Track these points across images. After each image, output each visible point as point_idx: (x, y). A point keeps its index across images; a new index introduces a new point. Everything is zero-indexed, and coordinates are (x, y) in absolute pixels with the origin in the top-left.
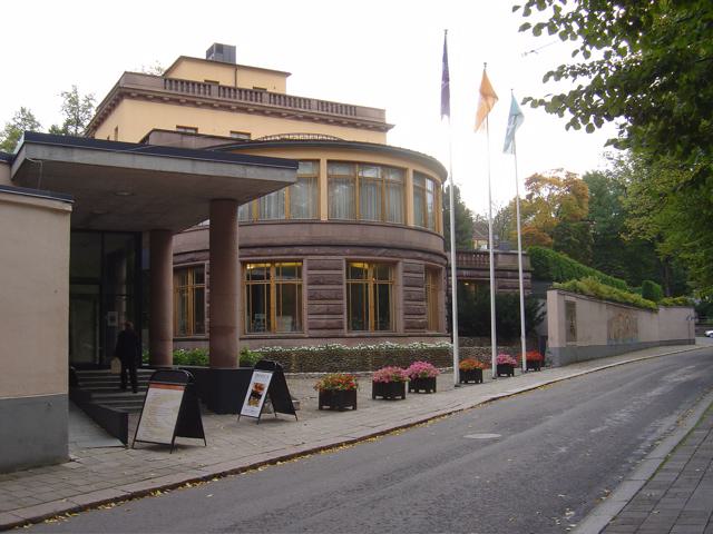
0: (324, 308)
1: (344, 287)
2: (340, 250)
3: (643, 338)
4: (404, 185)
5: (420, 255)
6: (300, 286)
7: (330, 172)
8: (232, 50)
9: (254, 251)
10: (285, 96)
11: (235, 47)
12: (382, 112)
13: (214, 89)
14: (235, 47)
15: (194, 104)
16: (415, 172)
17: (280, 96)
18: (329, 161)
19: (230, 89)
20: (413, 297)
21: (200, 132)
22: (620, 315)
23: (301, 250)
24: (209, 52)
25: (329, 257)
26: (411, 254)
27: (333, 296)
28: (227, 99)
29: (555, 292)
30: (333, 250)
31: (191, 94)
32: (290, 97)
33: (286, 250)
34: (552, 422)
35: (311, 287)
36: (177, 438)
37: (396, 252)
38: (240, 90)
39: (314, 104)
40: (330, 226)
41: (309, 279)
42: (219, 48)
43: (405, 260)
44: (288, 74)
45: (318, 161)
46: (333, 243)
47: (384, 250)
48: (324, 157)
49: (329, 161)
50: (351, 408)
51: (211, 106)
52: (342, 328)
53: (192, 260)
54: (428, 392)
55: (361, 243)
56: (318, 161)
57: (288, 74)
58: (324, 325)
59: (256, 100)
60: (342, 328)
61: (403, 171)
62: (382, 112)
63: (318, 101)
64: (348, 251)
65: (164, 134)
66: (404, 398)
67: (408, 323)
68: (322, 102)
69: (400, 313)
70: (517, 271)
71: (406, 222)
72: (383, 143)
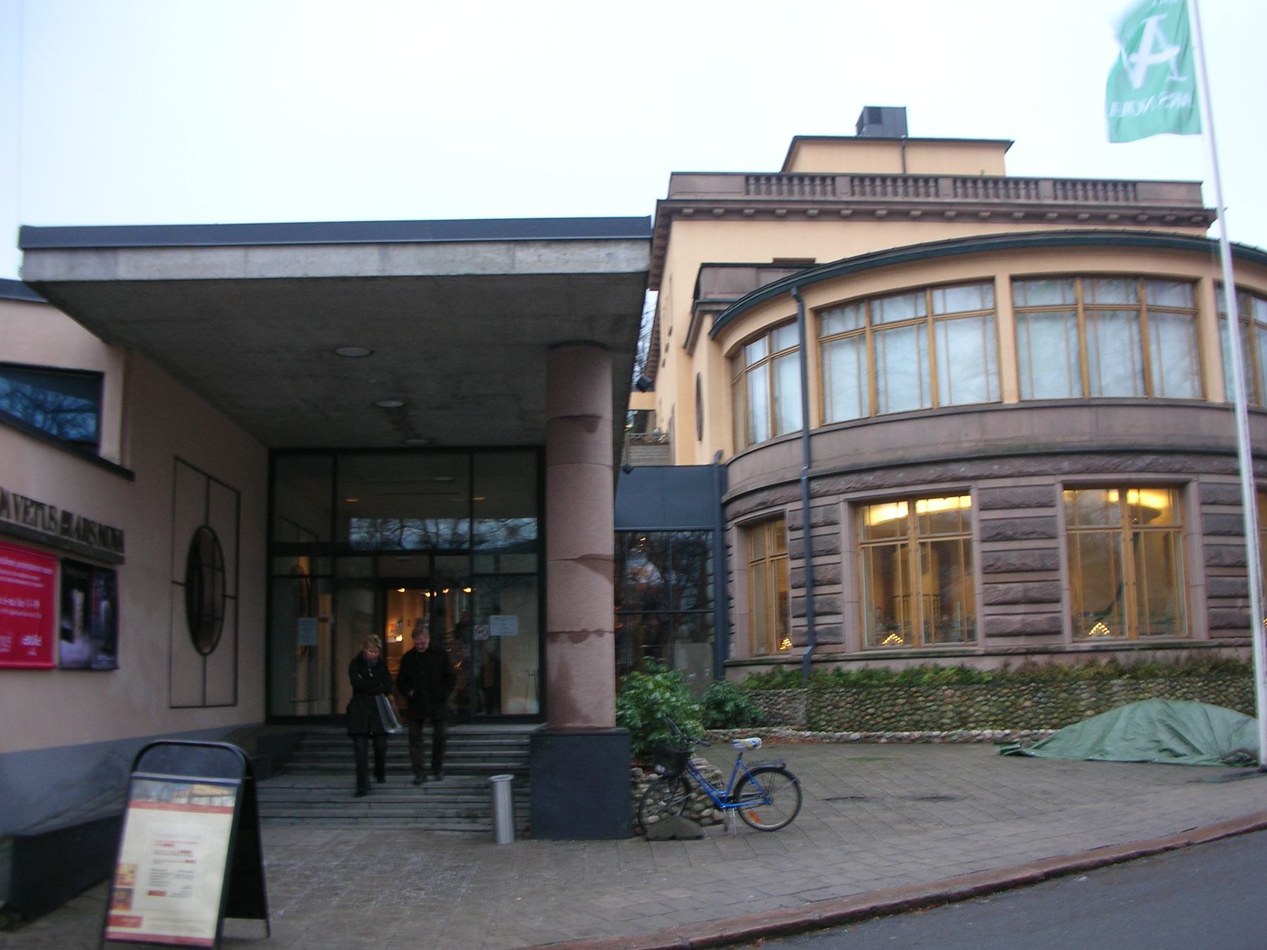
0: (1017, 590)
1: (1061, 543)
2: (1048, 465)
6: (968, 544)
7: (1020, 303)
9: (869, 478)
10: (1006, 181)
11: (903, 111)
14: (903, 111)
17: (996, 181)
18: (1014, 279)
19: (894, 179)
20: (1228, 561)
23: (962, 469)
24: (860, 125)
25: (1023, 481)
27: (1037, 565)
28: (869, 198)
30: (1033, 465)
31: (796, 197)
32: (1017, 181)
33: (932, 472)
34: (554, 945)
35: (989, 546)
36: (227, 921)
37: (1178, 462)
38: (916, 179)
39: (1046, 189)
40: (1023, 416)
41: (983, 530)
42: (873, 115)
43: (1205, 478)
45: (991, 280)
46: (1031, 450)
48: (1002, 271)
49: (1014, 279)
52: (1058, 632)
53: (765, 505)
55: (1095, 445)
56: (991, 280)
57: (1006, 145)
58: (1016, 627)
60: (1058, 632)
63: (1055, 182)
64: (1066, 464)
65: (723, 271)
67: (1215, 616)
68: (1064, 182)
69: (1199, 596)
70: (1233, 454)
71: (1204, 393)
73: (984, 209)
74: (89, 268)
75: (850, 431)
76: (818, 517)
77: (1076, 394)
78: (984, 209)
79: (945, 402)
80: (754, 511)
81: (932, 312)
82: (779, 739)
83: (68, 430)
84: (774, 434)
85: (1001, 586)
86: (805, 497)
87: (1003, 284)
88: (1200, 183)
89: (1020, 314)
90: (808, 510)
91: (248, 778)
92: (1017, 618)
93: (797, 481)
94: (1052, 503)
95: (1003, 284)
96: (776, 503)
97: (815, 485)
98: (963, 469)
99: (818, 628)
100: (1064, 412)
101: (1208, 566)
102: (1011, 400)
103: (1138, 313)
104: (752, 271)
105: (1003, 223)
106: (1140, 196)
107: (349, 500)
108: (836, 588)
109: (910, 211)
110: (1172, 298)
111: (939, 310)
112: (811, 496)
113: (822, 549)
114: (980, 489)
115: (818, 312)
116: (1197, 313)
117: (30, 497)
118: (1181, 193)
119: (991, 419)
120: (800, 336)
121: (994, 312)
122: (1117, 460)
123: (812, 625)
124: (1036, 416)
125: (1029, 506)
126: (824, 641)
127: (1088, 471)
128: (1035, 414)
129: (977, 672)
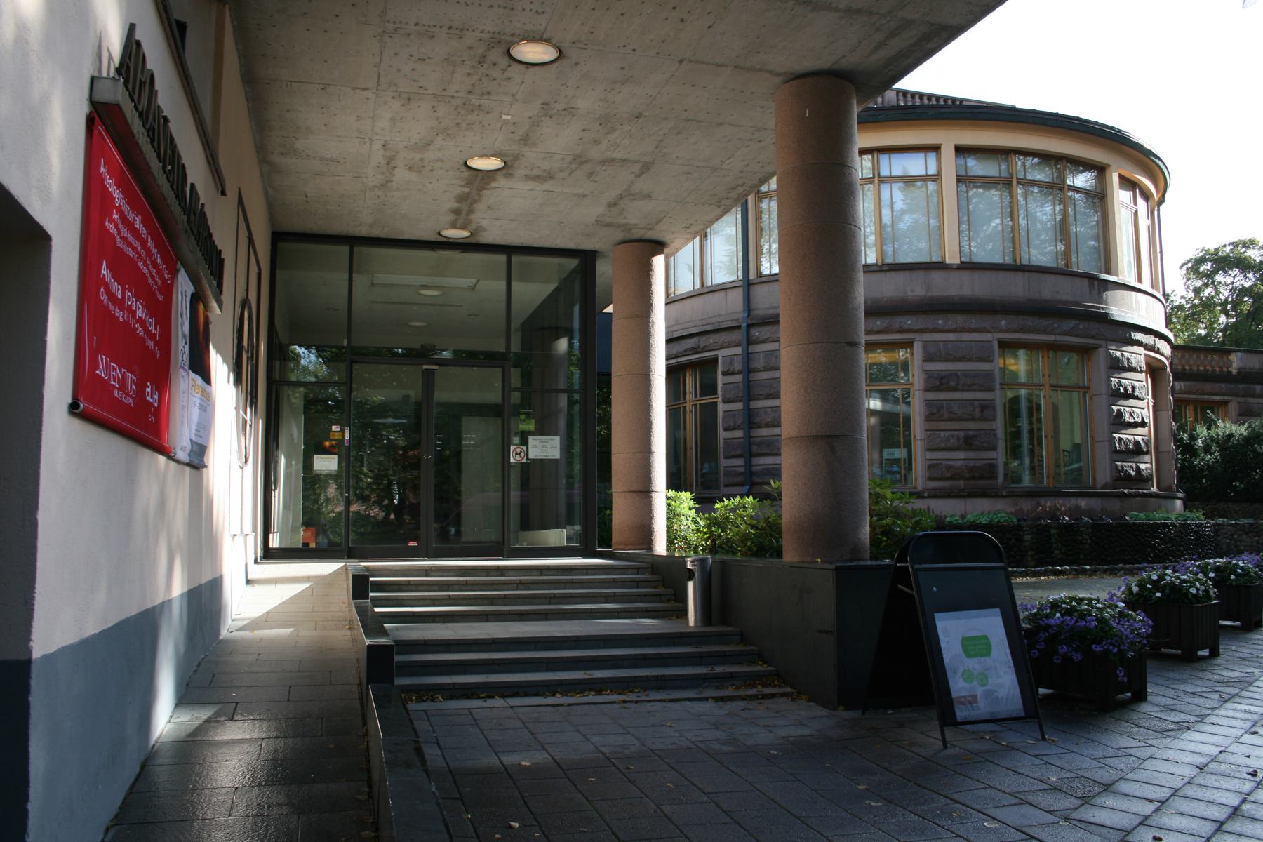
2: (987, 321)
23: (909, 322)
40: (966, 275)
45: (936, 149)
47: (1072, 323)
49: (961, 150)
74: (177, 34)
75: (684, 301)
76: (759, 362)
77: (1008, 260)
79: (889, 260)
80: (683, 356)
81: (879, 174)
84: (702, 284)
85: (942, 434)
86: (745, 343)
87: (948, 153)
89: (963, 180)
90: (748, 357)
91: (1017, 442)
92: (959, 458)
93: (739, 327)
94: (991, 358)
96: (707, 349)
97: (756, 332)
98: (909, 322)
99: (754, 469)
100: (1001, 274)
101: (1113, 424)
102: (952, 258)
108: (776, 431)
111: (885, 172)
112: (750, 342)
113: (761, 393)
114: (923, 341)
116: (1104, 197)
117: (954, 164)
119: (936, 276)
120: (1034, 151)
121: (936, 178)
122: (1045, 323)
123: (749, 465)
124: (977, 275)
125: (970, 360)
126: (760, 481)
127: (1021, 330)
128: (976, 274)
129: (918, 511)
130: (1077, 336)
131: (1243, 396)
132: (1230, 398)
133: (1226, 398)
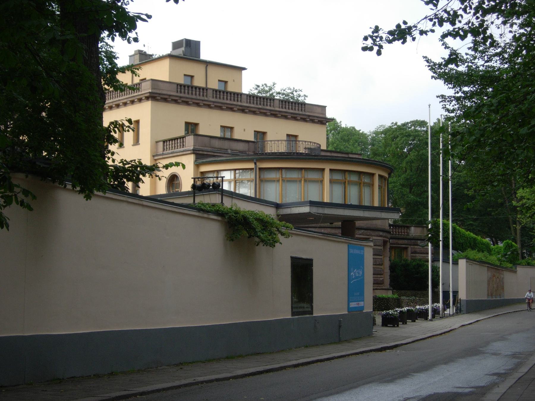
3: (507, 296)
4: (373, 185)
5: (381, 233)
8: (197, 44)
12: (324, 108)
13: (210, 93)
15: (198, 105)
16: (379, 176)
18: (331, 170)
21: (236, 136)
22: (494, 276)
26: (377, 233)
29: (464, 260)
37: (369, 232)
44: (244, 69)
45: (323, 170)
47: (363, 231)
48: (327, 167)
49: (331, 170)
50: (396, 326)
51: (209, 106)
54: (394, 326)
56: (323, 170)
57: (244, 69)
59: (238, 101)
61: (373, 175)
62: (324, 108)
66: (398, 326)
72: (240, 92)
73: (316, 119)
78: (316, 119)
82: (188, 127)
83: (118, 158)
87: (327, 173)
88: (326, 106)
95: (327, 173)
103: (359, 184)
104: (208, 139)
105: (217, 110)
106: (306, 110)
107: (112, 11)
109: (234, 108)
110: (366, 180)
115: (260, 169)
118: (319, 110)
130: (364, 235)
131: (413, 245)
132: (408, 246)
133: (407, 246)
